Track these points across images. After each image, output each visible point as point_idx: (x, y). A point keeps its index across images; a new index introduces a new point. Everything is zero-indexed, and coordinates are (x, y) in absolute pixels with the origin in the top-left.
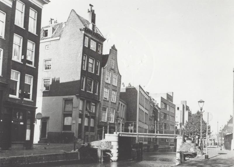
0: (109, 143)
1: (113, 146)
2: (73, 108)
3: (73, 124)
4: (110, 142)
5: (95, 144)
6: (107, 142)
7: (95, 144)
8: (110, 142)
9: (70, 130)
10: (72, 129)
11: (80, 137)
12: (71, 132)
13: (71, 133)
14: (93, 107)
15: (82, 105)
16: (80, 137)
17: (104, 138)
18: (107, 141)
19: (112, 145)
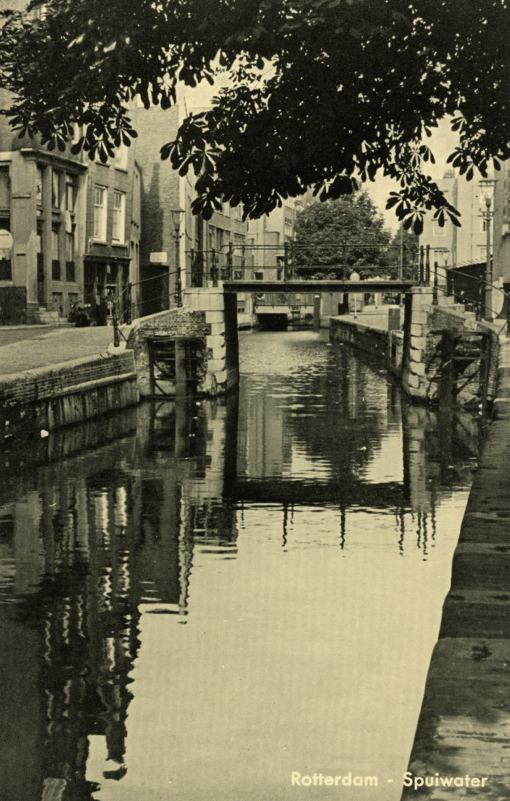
0: (198, 317)
1: (210, 326)
2: (10, 198)
3: (18, 255)
4: (203, 315)
5: (275, 58)
6: (193, 315)
7: (275, 58)
8: (203, 315)
9: (9, 277)
10: (16, 271)
11: (42, 302)
12: (11, 283)
13: (14, 288)
14: (110, 233)
15: (241, 439)
16: (42, 302)
17: (179, 300)
18: (194, 313)
19: (207, 321)
